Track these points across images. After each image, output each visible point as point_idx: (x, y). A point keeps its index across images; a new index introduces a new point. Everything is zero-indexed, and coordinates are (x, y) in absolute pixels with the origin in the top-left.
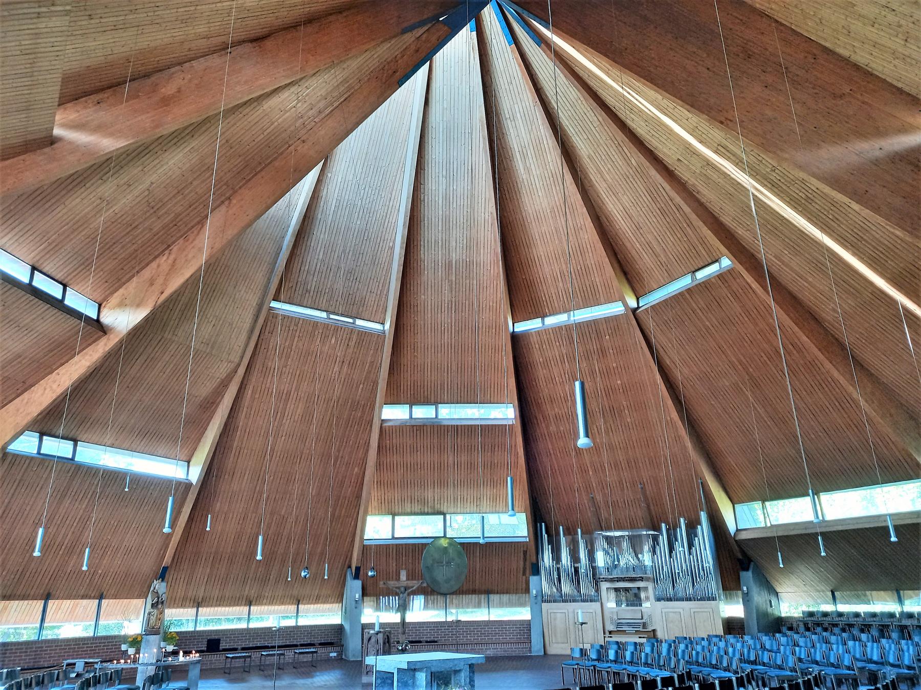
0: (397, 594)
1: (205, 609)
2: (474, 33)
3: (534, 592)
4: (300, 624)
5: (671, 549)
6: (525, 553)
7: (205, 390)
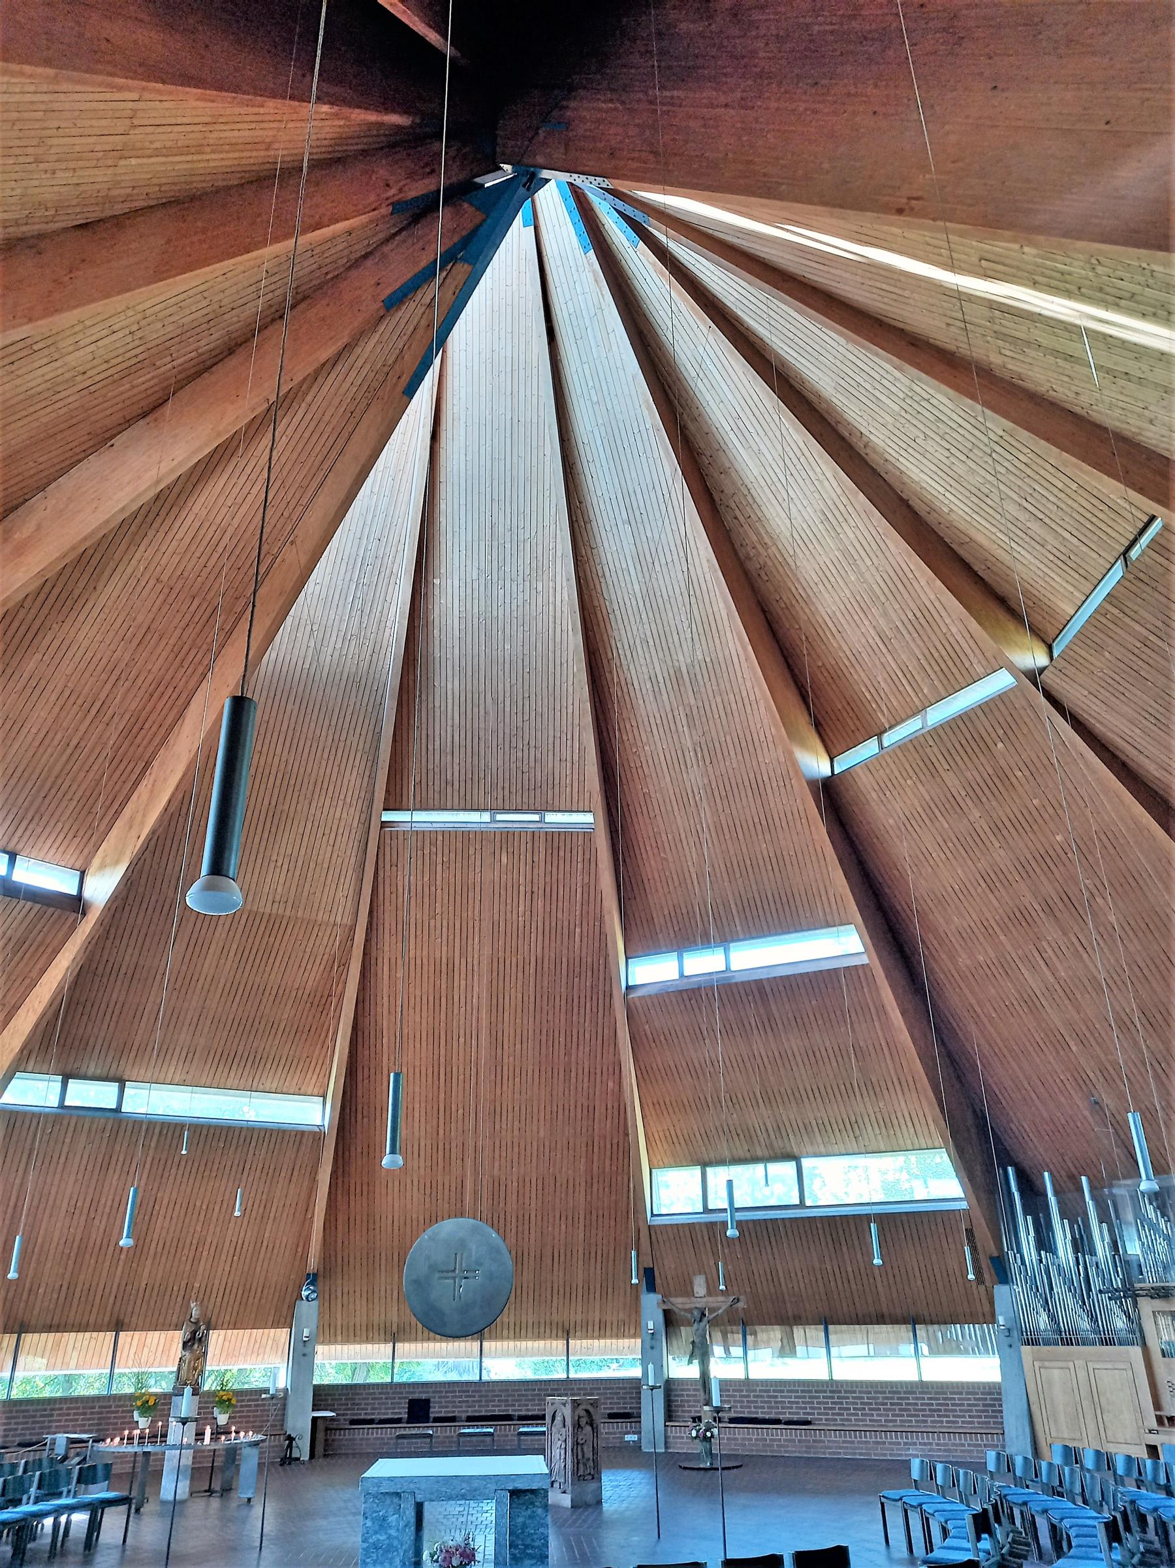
0: (690, 1324)
1: (407, 1345)
2: (592, 253)
3: (651, 1325)
4: (754, 1375)
6: (970, 1233)
7: (312, 977)
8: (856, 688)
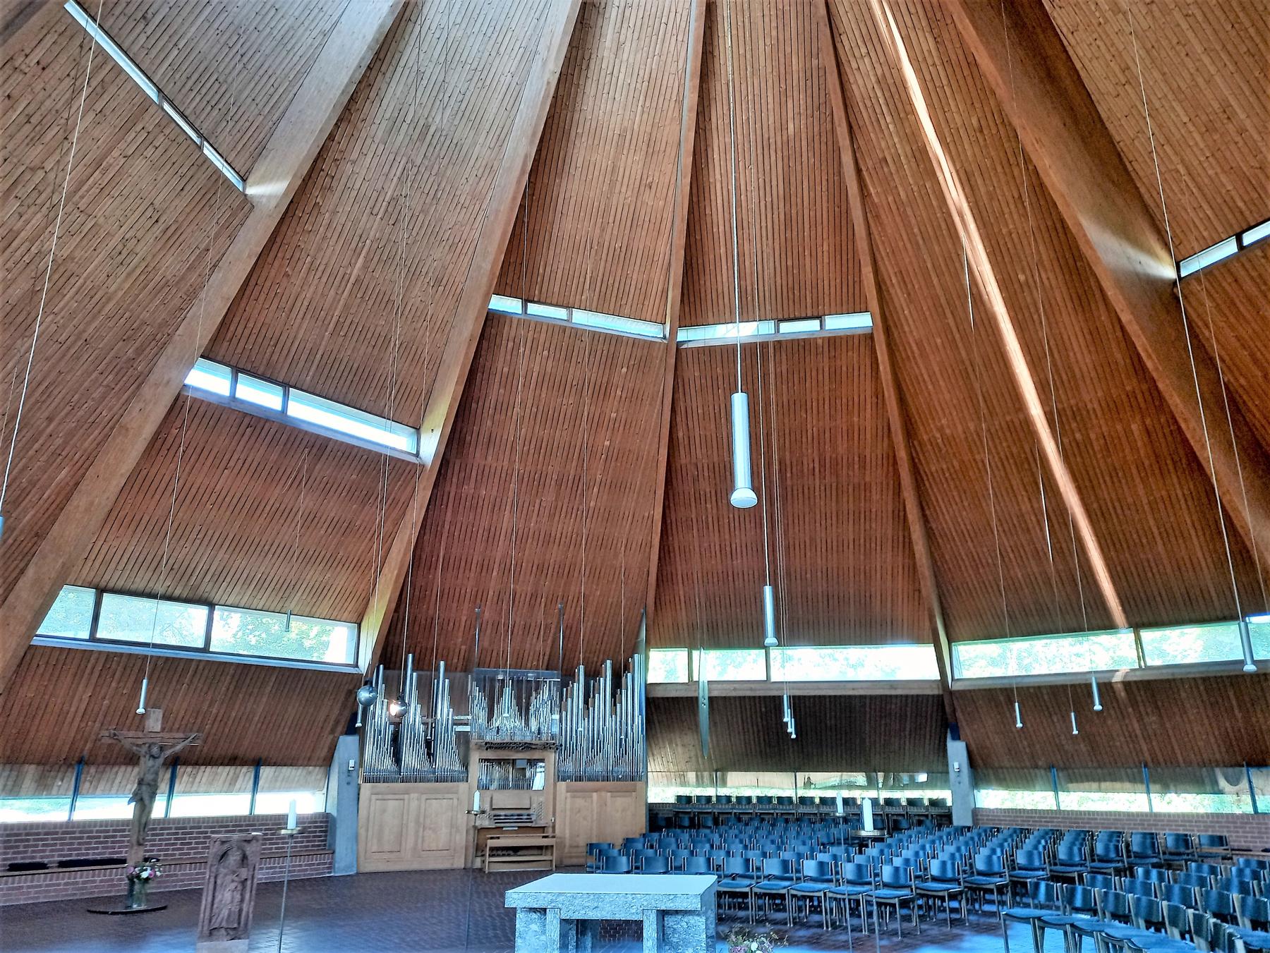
3: (956, 765)
8: (538, 258)
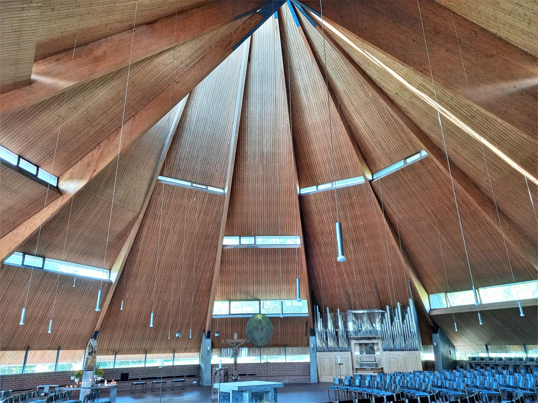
0: (232, 347)
1: (120, 356)
3: (312, 346)
4: (175, 364)
5: (392, 320)
6: (307, 323)
7: (120, 228)
